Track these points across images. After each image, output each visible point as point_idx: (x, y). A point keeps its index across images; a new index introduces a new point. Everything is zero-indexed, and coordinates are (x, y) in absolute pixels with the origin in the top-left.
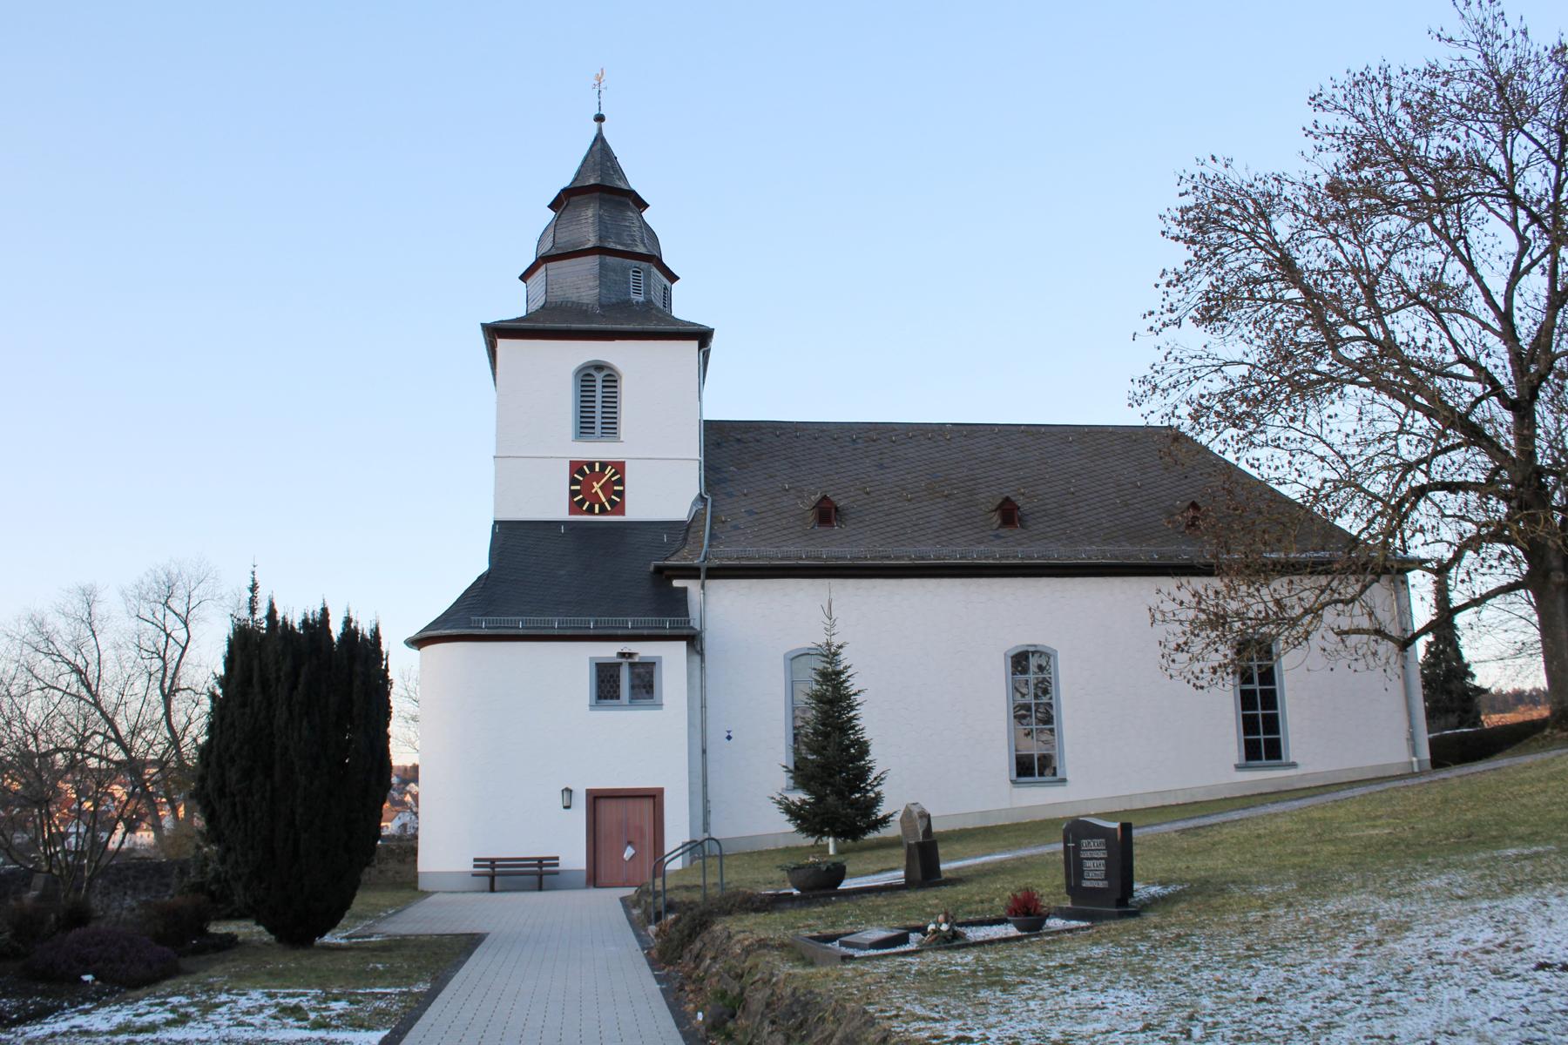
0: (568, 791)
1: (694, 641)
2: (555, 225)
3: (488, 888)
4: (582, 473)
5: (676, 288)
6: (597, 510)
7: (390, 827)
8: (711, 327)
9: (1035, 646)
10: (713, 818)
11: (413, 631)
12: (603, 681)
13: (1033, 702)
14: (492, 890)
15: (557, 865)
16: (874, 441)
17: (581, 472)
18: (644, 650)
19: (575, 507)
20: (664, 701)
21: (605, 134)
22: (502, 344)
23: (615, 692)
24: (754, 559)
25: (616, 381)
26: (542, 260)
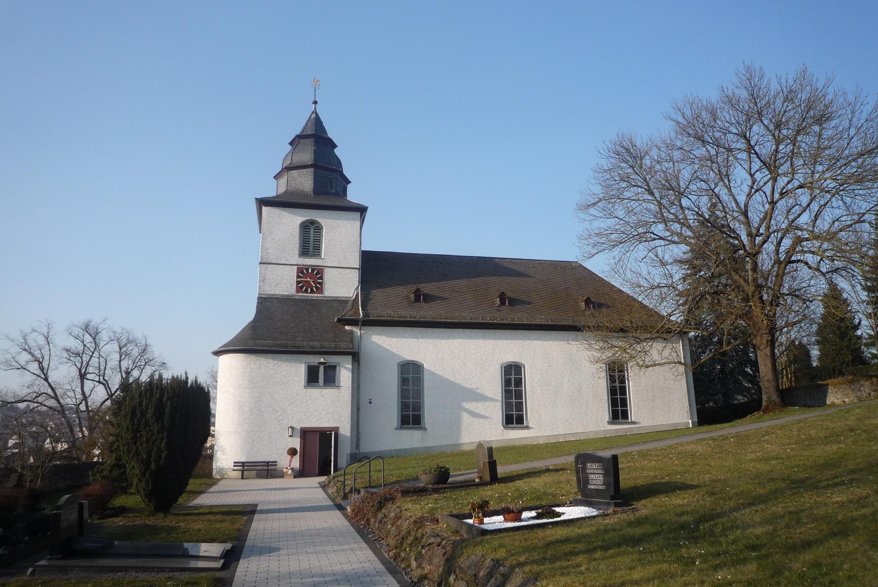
0: (292, 428)
1: (355, 357)
2: (292, 152)
3: (241, 477)
4: (318, 273)
5: (349, 186)
6: (309, 291)
7: (208, 445)
8: (367, 206)
9: (515, 362)
10: (361, 442)
11: (215, 349)
12: (311, 374)
13: (514, 389)
14: (243, 478)
15: (276, 465)
16: (441, 263)
17: (302, 271)
18: (333, 360)
19: (299, 289)
20: (341, 385)
21: (317, 111)
22: (265, 209)
23: (316, 379)
24: (384, 317)
25: (320, 230)
26: (288, 169)
